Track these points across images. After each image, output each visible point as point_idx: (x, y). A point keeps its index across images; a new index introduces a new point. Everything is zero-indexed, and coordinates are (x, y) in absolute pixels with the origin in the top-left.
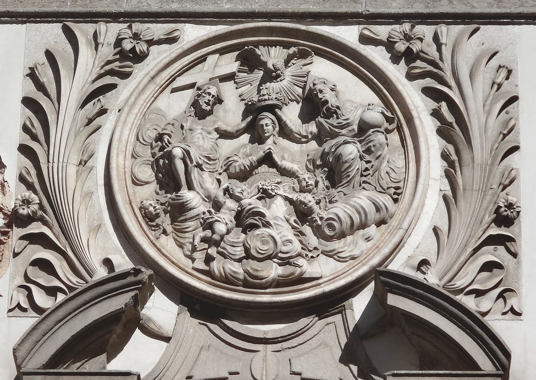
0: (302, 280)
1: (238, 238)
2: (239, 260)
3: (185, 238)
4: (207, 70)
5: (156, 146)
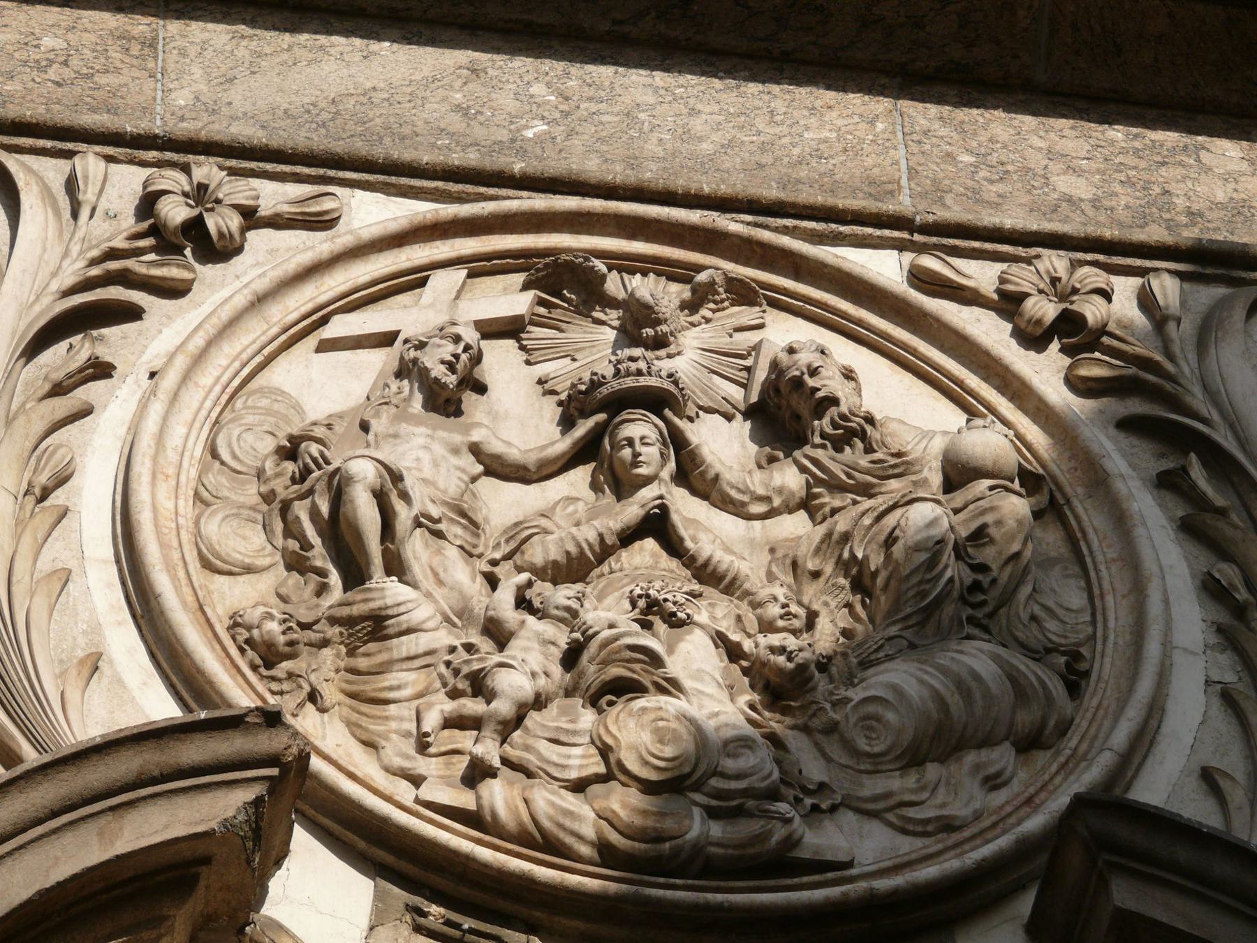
0: (784, 864)
1: (571, 721)
2: (579, 786)
3: (387, 718)
4: (432, 305)
5: (277, 475)
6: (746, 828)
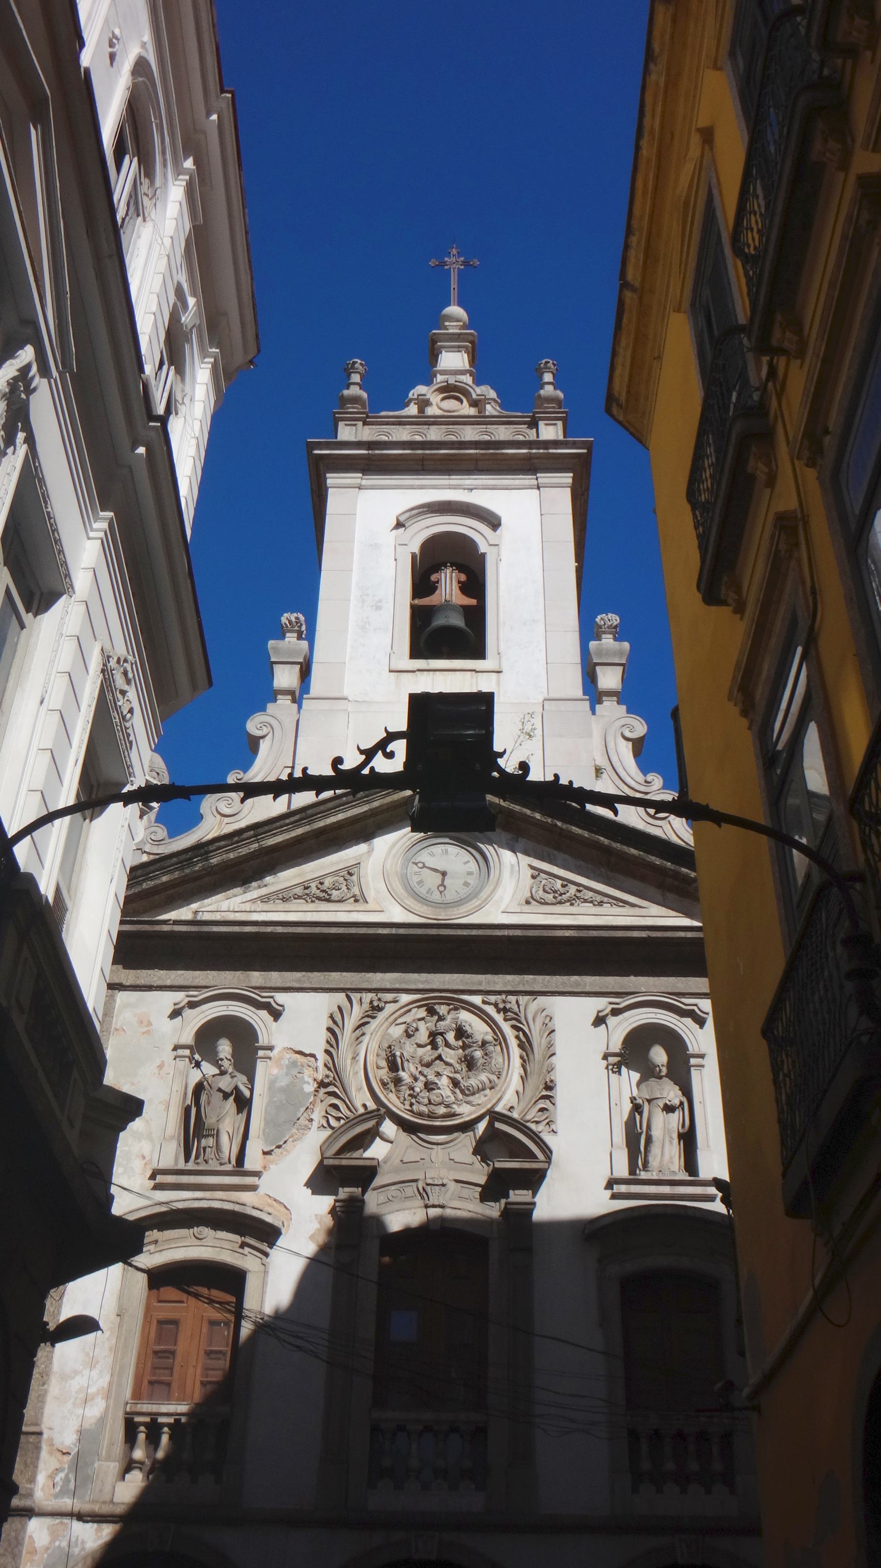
0: (454, 1115)
6: (449, 1110)
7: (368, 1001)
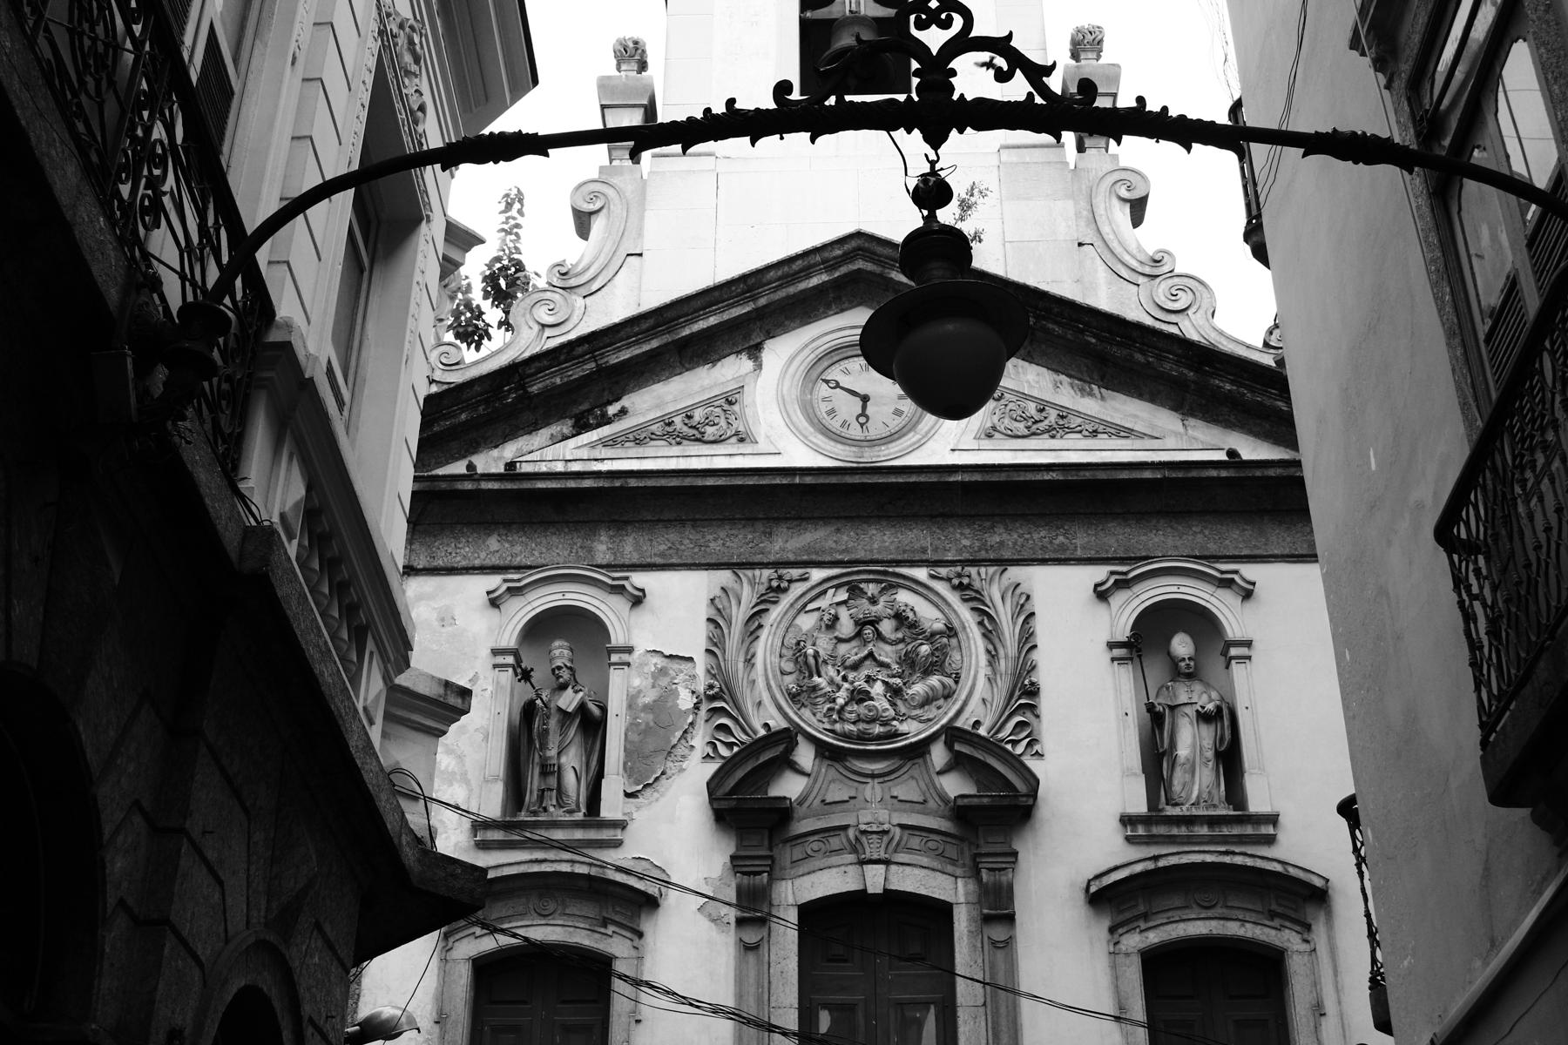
0: (895, 735)
7: (764, 579)
